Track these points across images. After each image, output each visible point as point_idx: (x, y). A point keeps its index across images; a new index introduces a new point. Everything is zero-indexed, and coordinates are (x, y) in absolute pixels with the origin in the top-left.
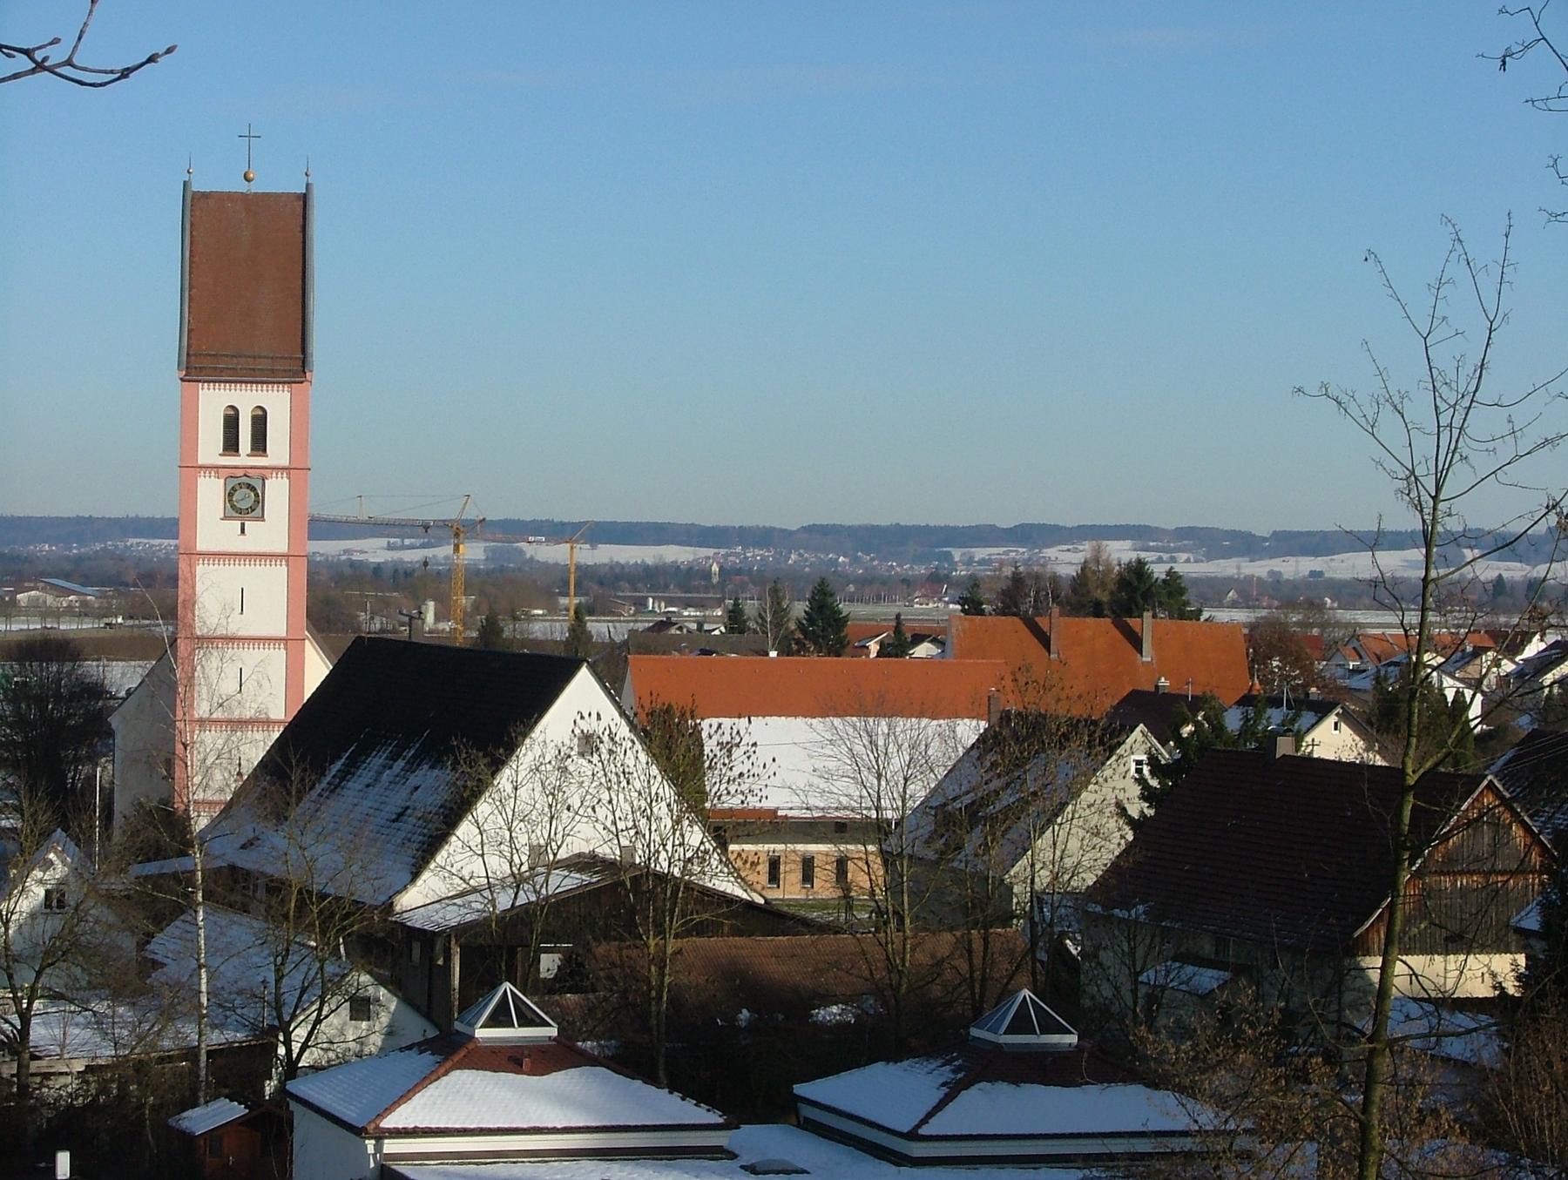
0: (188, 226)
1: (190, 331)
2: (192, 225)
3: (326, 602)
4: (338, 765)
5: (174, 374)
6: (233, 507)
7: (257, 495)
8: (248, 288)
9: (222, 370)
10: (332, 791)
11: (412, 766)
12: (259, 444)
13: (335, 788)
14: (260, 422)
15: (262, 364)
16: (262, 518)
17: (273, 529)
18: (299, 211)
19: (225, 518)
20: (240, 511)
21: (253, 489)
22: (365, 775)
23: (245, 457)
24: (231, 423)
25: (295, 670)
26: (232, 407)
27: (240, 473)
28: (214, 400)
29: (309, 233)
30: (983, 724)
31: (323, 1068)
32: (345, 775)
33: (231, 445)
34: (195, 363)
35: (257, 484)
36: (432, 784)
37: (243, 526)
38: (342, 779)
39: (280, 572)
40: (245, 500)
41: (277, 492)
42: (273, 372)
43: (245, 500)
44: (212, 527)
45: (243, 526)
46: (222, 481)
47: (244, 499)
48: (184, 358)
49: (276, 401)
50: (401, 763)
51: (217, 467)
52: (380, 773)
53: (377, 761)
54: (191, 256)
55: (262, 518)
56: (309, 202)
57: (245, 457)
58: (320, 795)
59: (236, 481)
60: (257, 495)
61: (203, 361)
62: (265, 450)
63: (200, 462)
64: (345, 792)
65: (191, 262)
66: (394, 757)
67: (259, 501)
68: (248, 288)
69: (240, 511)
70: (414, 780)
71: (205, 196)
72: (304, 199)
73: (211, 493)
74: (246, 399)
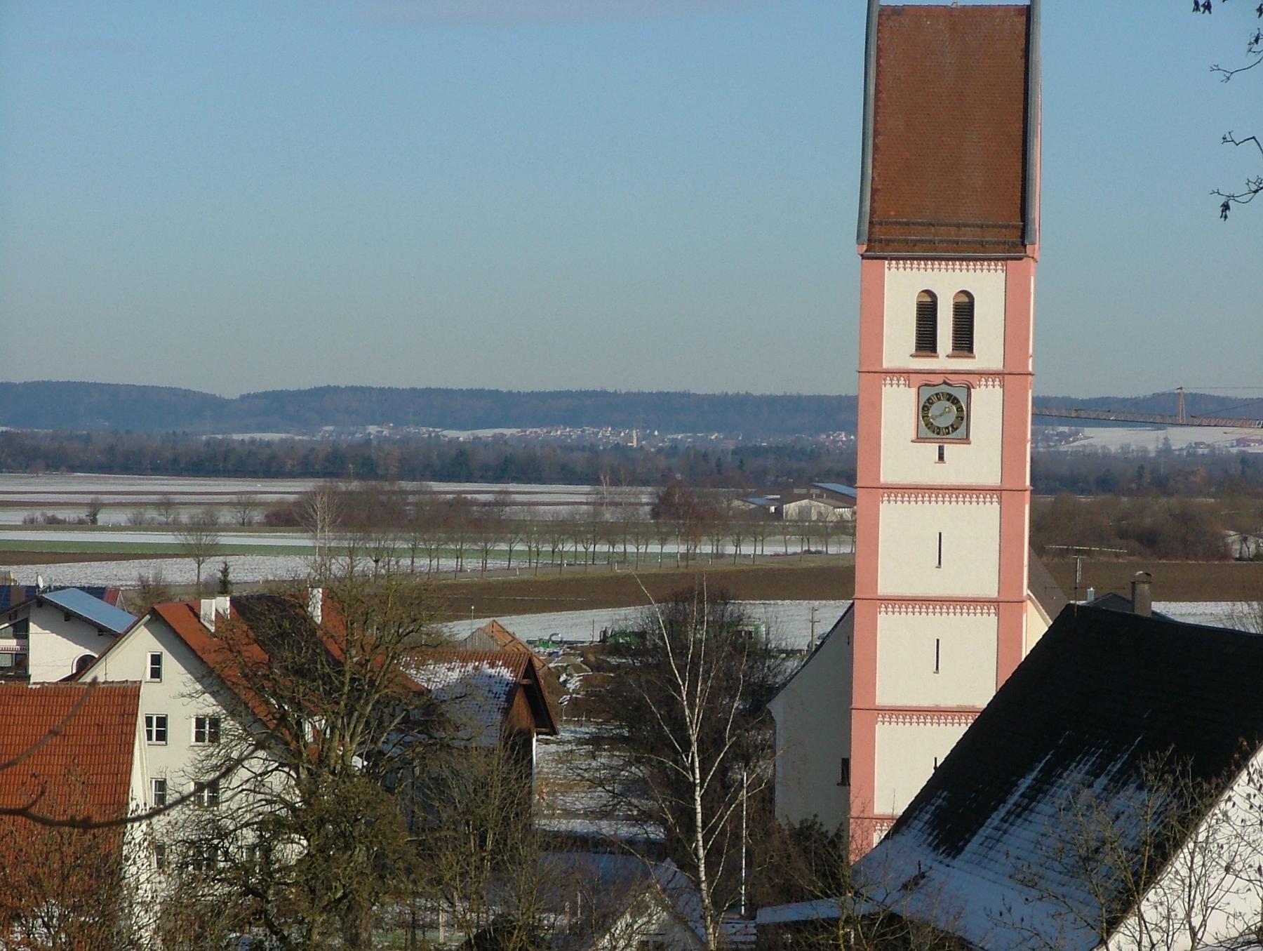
0: (873, 53)
1: (874, 191)
2: (879, 49)
3: (1070, 510)
4: (1026, 782)
5: (853, 250)
6: (929, 425)
7: (960, 409)
8: (951, 153)
9: (915, 243)
10: (1019, 816)
11: (1119, 781)
12: (964, 340)
13: (1022, 811)
14: (965, 312)
15: (968, 235)
16: (966, 440)
17: (981, 456)
18: (1021, 28)
19: (919, 439)
20: (937, 430)
21: (955, 401)
22: (1060, 794)
23: (944, 359)
24: (927, 312)
25: (1009, 633)
26: (928, 292)
27: (938, 379)
28: (903, 283)
29: (1033, 57)
30: (853, 858)
31: (819, 648)
32: (1034, 794)
33: (926, 342)
34: (879, 233)
35: (961, 395)
36: (1141, 806)
37: (941, 450)
38: (1032, 799)
39: (990, 512)
40: (944, 417)
41: (986, 406)
42: (982, 245)
43: (944, 417)
44: (898, 448)
45: (941, 450)
46: (914, 391)
47: (943, 414)
48: (866, 227)
49: (987, 283)
50: (1103, 781)
51: (908, 372)
52: (1076, 793)
53: (1074, 776)
54: (877, 91)
55: (966, 440)
56: (1035, 19)
57: (944, 359)
58: (1004, 820)
59: (934, 391)
60: (960, 409)
61: (890, 233)
62: (970, 349)
63: (886, 365)
64: (1032, 817)
65: (877, 99)
66: (1096, 773)
67: (963, 416)
68: (951, 153)
69: (937, 430)
70: (1119, 802)
71: (897, 11)
72: (1028, 13)
73: (898, 408)
74: (947, 281)
